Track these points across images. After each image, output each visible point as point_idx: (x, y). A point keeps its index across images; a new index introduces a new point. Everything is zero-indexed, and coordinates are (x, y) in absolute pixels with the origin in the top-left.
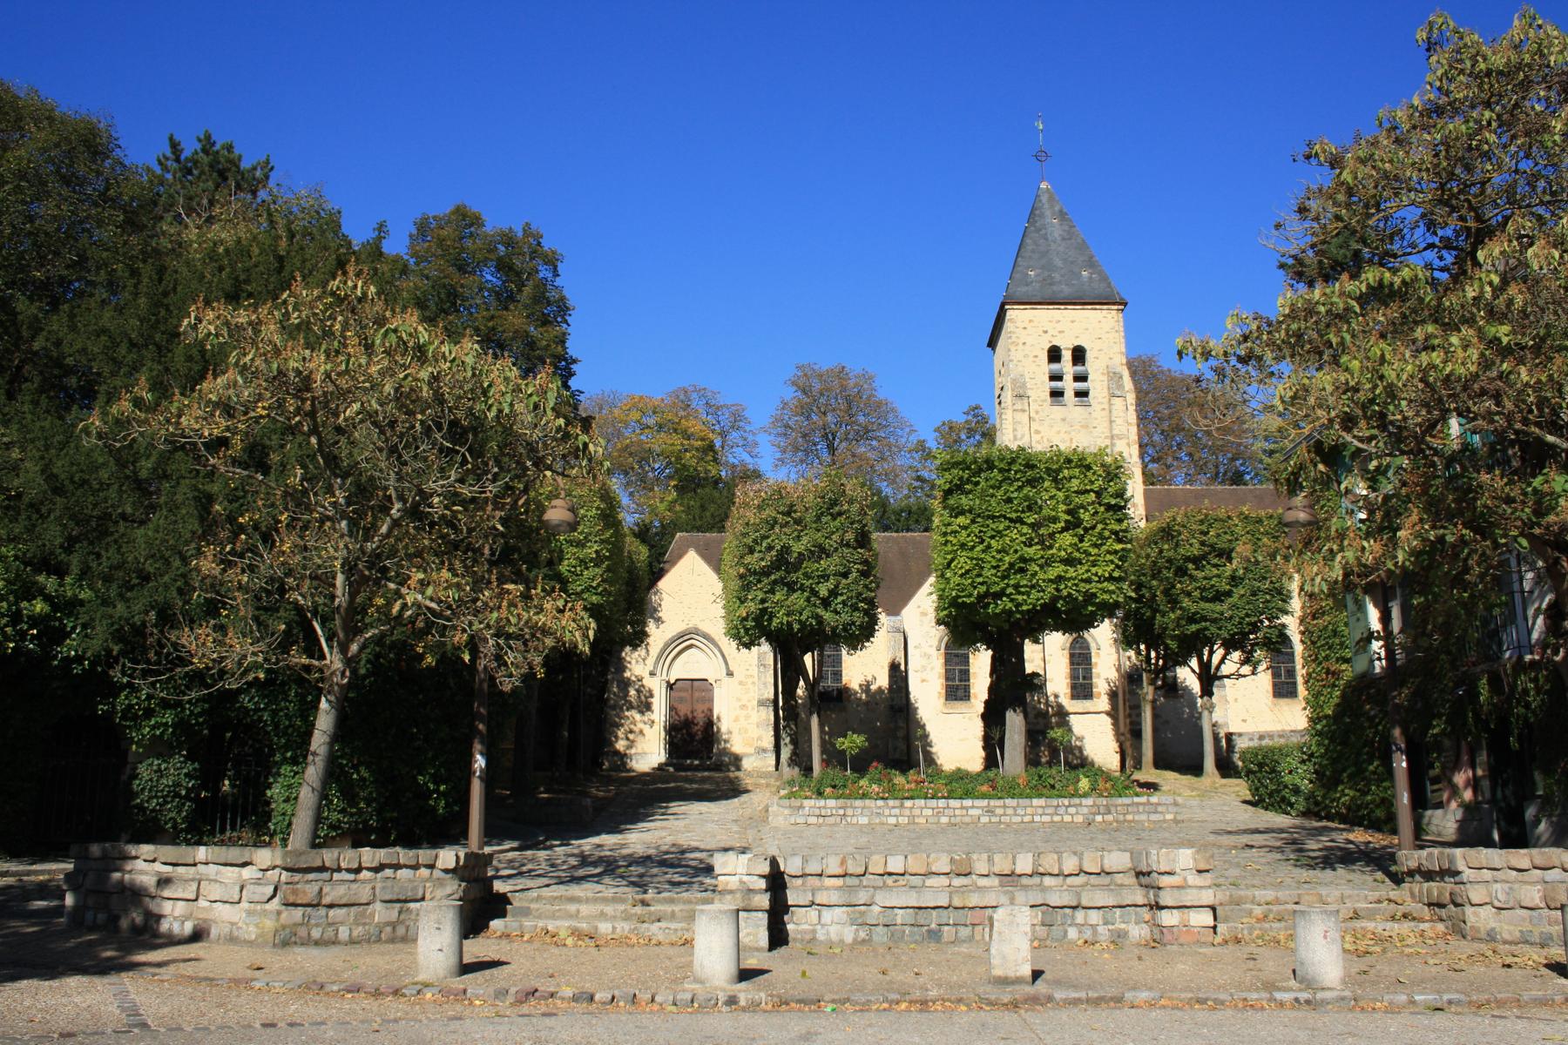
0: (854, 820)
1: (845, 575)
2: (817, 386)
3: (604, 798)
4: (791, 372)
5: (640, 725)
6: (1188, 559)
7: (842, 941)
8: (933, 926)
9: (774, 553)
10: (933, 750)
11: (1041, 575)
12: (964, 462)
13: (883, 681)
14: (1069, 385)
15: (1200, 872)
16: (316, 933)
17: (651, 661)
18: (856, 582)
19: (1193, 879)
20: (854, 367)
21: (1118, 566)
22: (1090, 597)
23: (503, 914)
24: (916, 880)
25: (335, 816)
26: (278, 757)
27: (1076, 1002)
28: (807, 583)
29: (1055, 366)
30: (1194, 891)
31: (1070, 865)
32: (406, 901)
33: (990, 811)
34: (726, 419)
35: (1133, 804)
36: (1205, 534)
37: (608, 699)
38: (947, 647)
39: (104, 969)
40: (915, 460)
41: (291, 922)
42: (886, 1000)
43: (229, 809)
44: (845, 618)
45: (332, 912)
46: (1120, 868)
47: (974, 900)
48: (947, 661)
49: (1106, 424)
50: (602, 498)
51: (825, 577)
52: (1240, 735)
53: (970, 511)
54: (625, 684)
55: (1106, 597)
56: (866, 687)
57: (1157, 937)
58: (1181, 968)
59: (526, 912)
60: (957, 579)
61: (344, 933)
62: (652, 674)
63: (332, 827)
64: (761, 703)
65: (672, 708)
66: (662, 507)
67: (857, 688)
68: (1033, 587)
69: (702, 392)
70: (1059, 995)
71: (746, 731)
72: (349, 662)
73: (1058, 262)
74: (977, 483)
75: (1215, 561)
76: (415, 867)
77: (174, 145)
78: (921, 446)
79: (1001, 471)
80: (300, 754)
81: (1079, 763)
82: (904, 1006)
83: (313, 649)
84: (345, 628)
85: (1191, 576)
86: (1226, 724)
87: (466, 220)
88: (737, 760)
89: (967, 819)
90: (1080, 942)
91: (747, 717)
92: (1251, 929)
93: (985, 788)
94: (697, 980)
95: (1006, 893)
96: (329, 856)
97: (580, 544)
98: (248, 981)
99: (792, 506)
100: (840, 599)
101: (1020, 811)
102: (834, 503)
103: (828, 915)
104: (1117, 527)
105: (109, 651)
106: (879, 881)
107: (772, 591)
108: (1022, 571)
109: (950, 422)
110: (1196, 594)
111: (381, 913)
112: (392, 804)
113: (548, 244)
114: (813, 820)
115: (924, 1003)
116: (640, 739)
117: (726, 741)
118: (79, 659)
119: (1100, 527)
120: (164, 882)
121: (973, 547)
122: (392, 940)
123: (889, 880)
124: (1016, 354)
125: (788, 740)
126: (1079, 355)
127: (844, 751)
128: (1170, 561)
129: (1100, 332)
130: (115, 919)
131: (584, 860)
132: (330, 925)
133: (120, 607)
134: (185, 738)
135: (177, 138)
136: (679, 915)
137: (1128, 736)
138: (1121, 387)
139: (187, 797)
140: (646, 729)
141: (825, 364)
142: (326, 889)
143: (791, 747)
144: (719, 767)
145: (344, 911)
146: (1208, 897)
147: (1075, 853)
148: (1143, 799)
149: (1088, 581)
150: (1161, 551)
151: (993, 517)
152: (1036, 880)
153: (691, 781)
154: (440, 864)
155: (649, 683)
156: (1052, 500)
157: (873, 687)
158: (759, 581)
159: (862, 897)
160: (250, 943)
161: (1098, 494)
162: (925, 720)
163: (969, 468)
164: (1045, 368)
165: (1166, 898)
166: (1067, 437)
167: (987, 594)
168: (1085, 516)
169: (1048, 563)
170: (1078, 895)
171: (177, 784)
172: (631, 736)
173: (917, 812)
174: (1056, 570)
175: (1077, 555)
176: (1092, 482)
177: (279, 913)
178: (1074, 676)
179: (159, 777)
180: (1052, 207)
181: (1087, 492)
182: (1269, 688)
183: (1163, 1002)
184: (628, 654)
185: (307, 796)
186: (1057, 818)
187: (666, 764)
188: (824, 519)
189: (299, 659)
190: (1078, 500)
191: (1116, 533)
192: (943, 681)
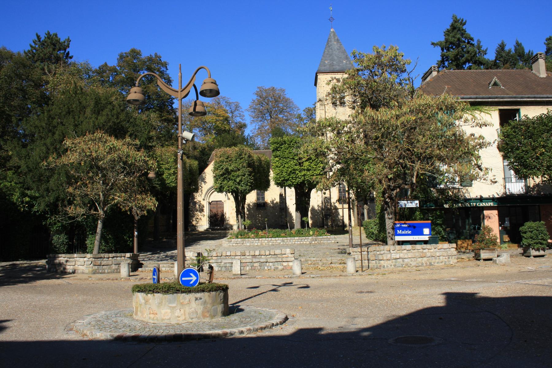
1: (244, 175)
2: (264, 94)
4: (256, 90)
5: (200, 216)
13: (278, 200)
16: (100, 271)
17: (203, 196)
18: (247, 177)
19: (290, 255)
20: (277, 87)
23: (141, 267)
24: (233, 257)
25: (103, 248)
26: (88, 233)
33: (283, 241)
39: (58, 278)
43: (78, 246)
44: (244, 188)
51: (238, 176)
54: (195, 203)
56: (272, 202)
59: (147, 267)
61: (106, 271)
62: (204, 200)
63: (103, 250)
66: (210, 140)
72: (105, 212)
73: (336, 58)
76: (121, 257)
77: (38, 37)
80: (94, 232)
83: (96, 210)
84: (103, 205)
87: (135, 53)
96: (102, 255)
97: (169, 169)
98: (88, 279)
105: (45, 209)
106: (225, 257)
111: (114, 267)
112: (116, 243)
113: (163, 60)
114: (234, 245)
118: (38, 211)
120: (67, 261)
122: (117, 272)
130: (57, 270)
131: (167, 256)
133: (47, 198)
134: (64, 229)
135: (39, 34)
139: (66, 244)
140: (202, 217)
148: (329, 237)
151: (285, 158)
155: (203, 203)
157: (275, 202)
159: (219, 261)
160: (87, 273)
171: (63, 241)
179: (59, 239)
184: (196, 195)
185: (97, 243)
189: (93, 212)
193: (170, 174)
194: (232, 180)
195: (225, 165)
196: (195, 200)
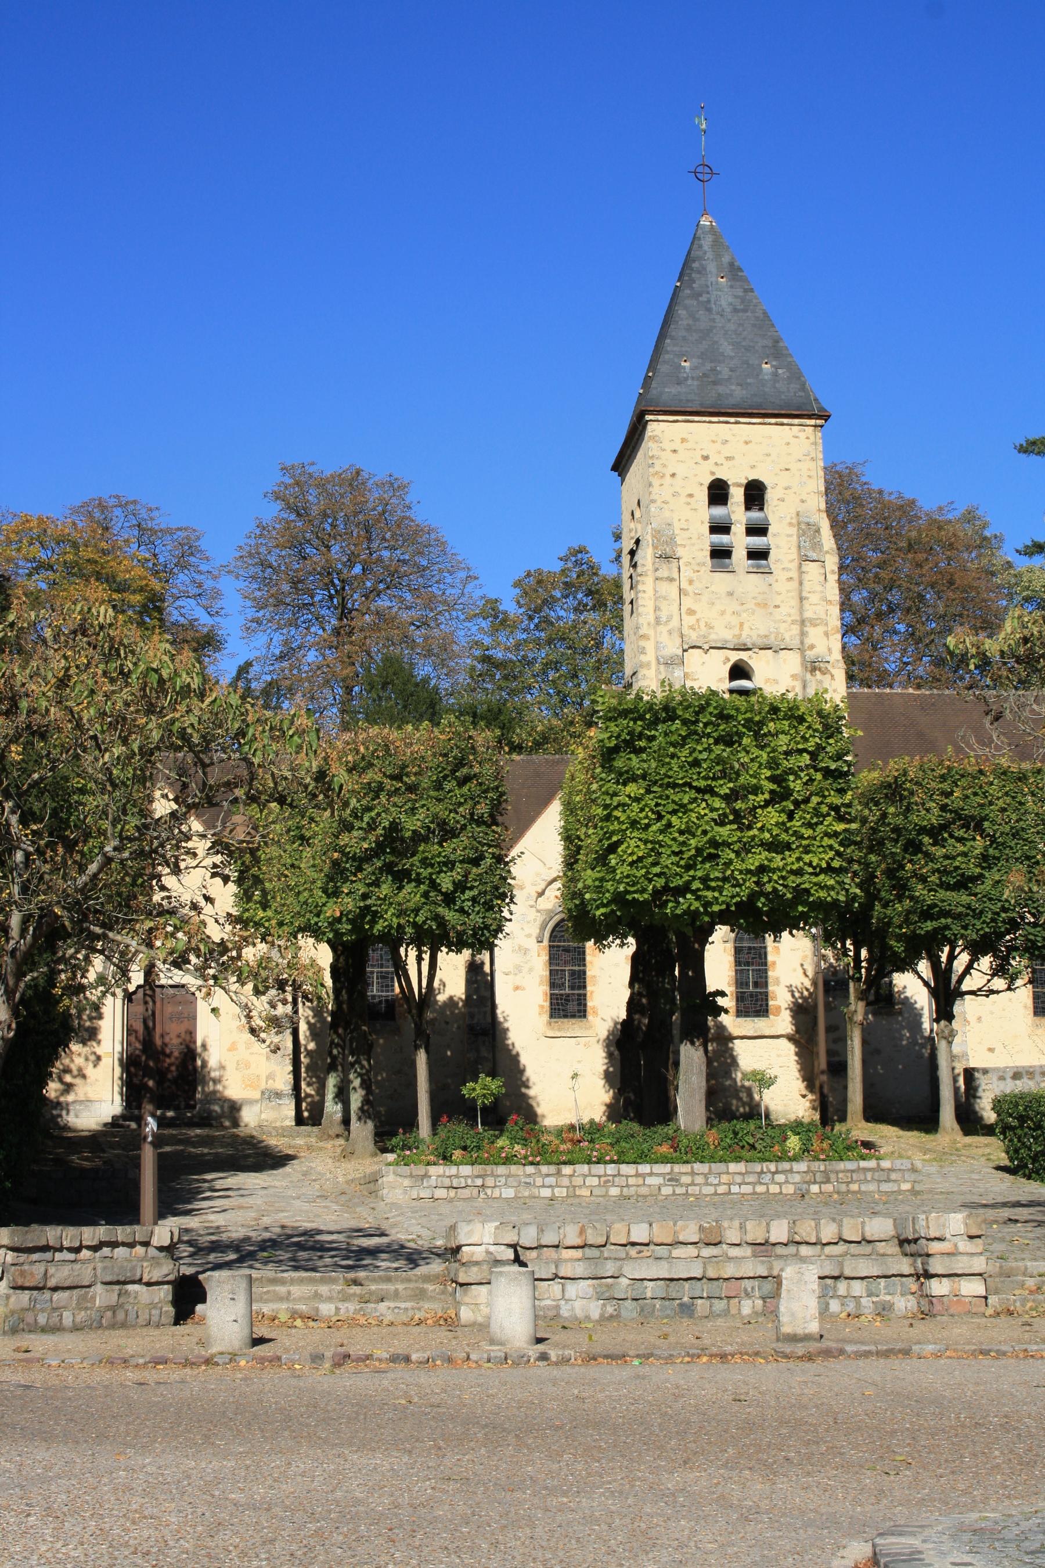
0: (496, 1193)
4: (274, 479)
5: (79, 1061)
6: (922, 830)
7: (588, 1318)
8: (686, 1299)
9: (380, 831)
10: (531, 1092)
11: (738, 865)
12: (635, 710)
14: (739, 541)
15: (971, 1237)
16: (42, 1320)
19: (964, 1245)
20: (377, 469)
21: (838, 854)
22: (800, 893)
24: (661, 1251)
27: (867, 1354)
28: (425, 873)
29: (719, 511)
30: (965, 1258)
31: (828, 1232)
32: (125, 1283)
33: (673, 1179)
35: (859, 1169)
36: (948, 794)
40: (478, 630)
41: (18, 1307)
42: (688, 1355)
45: (56, 1296)
46: (883, 1237)
47: (729, 1271)
48: (553, 959)
49: (795, 602)
51: (450, 864)
52: (985, 1071)
53: (644, 777)
55: (822, 894)
57: (925, 1309)
58: (960, 1331)
60: (626, 869)
61: (67, 1319)
68: (725, 879)
70: (849, 1348)
71: (248, 1066)
73: (726, 348)
74: (652, 738)
75: (961, 833)
76: (131, 1245)
78: (492, 611)
79: (685, 722)
81: (732, 1105)
82: (705, 1359)
85: (927, 854)
86: (965, 1055)
88: (234, 1109)
89: (644, 1191)
90: (843, 1315)
92: (1024, 1302)
93: (665, 1149)
94: (492, 1342)
95: (763, 1262)
99: (404, 767)
100: (469, 894)
102: (460, 763)
103: (572, 1289)
104: (837, 801)
106: (621, 1252)
107: (376, 884)
109: (539, 572)
110: (934, 879)
114: (441, 1193)
115: (723, 1357)
117: (215, 1081)
119: (815, 800)
121: (648, 826)
122: (113, 1326)
123: (633, 1251)
124: (661, 491)
125: (357, 1082)
126: (755, 494)
127: (474, 1100)
128: (896, 830)
129: (787, 459)
132: (54, 1309)
136: (402, 1293)
137: (824, 1075)
138: (817, 545)
141: (329, 464)
142: (52, 1270)
144: (206, 1120)
145: (66, 1294)
146: (979, 1264)
147: (834, 1220)
149: (799, 872)
150: (884, 815)
151: (674, 786)
152: (792, 1249)
154: (155, 1242)
156: (752, 761)
158: (360, 869)
159: (610, 1268)
161: (814, 756)
162: (518, 1048)
163: (642, 717)
164: (704, 513)
165: (936, 1266)
166: (735, 621)
167: (666, 889)
168: (796, 785)
169: (746, 848)
170: (841, 1264)
173: (578, 1181)
174: (758, 858)
175: (784, 837)
176: (805, 739)
177: (8, 1297)
178: (555, 981)
181: (800, 752)
182: (1030, 1002)
183: (948, 1353)
186: (760, 1189)
187: (123, 1117)
188: (447, 786)
190: (792, 762)
191: (836, 809)
192: (546, 988)
194: (419, 881)
195: (390, 811)
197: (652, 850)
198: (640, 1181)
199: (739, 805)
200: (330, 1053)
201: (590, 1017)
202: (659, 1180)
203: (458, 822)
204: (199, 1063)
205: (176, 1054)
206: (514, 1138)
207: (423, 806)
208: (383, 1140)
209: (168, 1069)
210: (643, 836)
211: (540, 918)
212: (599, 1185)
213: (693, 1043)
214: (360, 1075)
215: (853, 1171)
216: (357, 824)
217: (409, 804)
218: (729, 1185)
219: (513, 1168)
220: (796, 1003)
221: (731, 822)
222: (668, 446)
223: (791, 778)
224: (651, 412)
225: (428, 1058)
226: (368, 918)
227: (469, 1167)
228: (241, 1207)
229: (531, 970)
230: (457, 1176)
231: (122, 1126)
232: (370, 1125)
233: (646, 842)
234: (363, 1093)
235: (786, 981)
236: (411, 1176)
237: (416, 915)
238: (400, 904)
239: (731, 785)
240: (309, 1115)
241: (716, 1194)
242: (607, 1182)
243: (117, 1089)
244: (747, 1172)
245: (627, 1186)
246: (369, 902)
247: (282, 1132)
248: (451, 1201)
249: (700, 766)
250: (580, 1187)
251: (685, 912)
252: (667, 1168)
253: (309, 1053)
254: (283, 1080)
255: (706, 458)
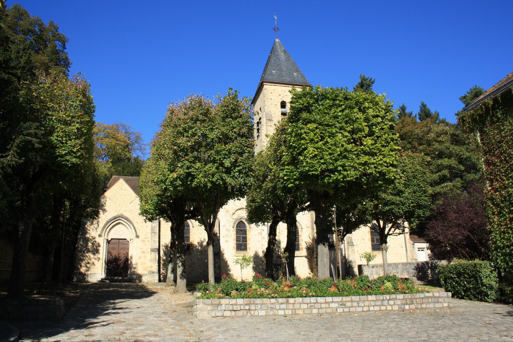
0: (256, 313)
3: (73, 297)
10: (231, 273)
17: (99, 230)
29: (283, 110)
33: (343, 304)
34: (133, 137)
37: (78, 247)
38: (237, 227)
48: (237, 233)
50: (84, 96)
54: (87, 240)
62: (100, 236)
64: (152, 250)
65: (109, 252)
67: (197, 244)
69: (124, 126)
71: (144, 264)
88: (140, 277)
89: (329, 311)
91: (145, 257)
97: (67, 123)
101: (361, 304)
108: (345, 157)
116: (92, 267)
117: (135, 268)
125: (180, 264)
140: (96, 262)
143: (182, 268)
144: (131, 280)
148: (430, 295)
151: (328, 125)
153: (121, 287)
155: (98, 240)
164: (280, 110)
168: (376, 130)
172: (88, 265)
173: (297, 306)
180: (281, 48)
186: (383, 308)
187: (105, 279)
190: (374, 120)
193: (68, 135)
196: (88, 236)
197: (320, 152)
198: (327, 306)
199: (354, 136)
200: (170, 257)
201: (248, 250)
202: (336, 305)
203: (233, 135)
204: (129, 262)
205: (123, 260)
206: (261, 285)
207: (217, 128)
208: (191, 287)
209: (120, 264)
210: (316, 146)
211: (234, 221)
212: (308, 308)
213: (324, 245)
214: (181, 261)
215: (423, 298)
216: (186, 134)
217: (211, 126)
218: (369, 306)
219: (265, 300)
220: (307, 247)
221: (352, 143)
222: (270, 92)
223: (374, 127)
224: (265, 82)
225: (213, 250)
226: (190, 178)
227: (242, 299)
228: (119, 322)
229: (231, 236)
230: (236, 305)
231: (104, 282)
232: (185, 280)
233: (317, 149)
234: (182, 268)
235: (304, 240)
236: (212, 304)
237: (213, 177)
238: (206, 172)
239: (352, 127)
240: (162, 279)
241: (363, 311)
242: (311, 307)
243: (103, 270)
244: (377, 300)
245: (321, 308)
246: (190, 170)
247: (154, 284)
248: (233, 317)
249: (338, 118)
250: (298, 309)
251: (333, 182)
252: (339, 299)
253: (163, 260)
254: (155, 268)
255: (280, 95)
